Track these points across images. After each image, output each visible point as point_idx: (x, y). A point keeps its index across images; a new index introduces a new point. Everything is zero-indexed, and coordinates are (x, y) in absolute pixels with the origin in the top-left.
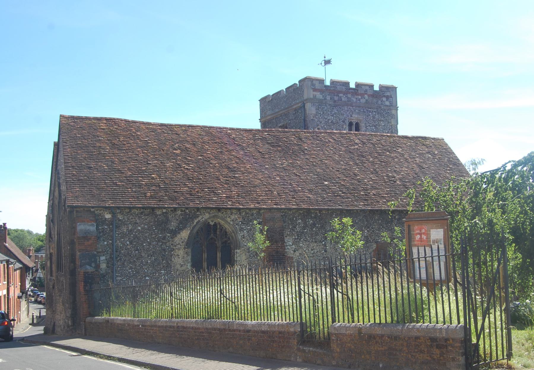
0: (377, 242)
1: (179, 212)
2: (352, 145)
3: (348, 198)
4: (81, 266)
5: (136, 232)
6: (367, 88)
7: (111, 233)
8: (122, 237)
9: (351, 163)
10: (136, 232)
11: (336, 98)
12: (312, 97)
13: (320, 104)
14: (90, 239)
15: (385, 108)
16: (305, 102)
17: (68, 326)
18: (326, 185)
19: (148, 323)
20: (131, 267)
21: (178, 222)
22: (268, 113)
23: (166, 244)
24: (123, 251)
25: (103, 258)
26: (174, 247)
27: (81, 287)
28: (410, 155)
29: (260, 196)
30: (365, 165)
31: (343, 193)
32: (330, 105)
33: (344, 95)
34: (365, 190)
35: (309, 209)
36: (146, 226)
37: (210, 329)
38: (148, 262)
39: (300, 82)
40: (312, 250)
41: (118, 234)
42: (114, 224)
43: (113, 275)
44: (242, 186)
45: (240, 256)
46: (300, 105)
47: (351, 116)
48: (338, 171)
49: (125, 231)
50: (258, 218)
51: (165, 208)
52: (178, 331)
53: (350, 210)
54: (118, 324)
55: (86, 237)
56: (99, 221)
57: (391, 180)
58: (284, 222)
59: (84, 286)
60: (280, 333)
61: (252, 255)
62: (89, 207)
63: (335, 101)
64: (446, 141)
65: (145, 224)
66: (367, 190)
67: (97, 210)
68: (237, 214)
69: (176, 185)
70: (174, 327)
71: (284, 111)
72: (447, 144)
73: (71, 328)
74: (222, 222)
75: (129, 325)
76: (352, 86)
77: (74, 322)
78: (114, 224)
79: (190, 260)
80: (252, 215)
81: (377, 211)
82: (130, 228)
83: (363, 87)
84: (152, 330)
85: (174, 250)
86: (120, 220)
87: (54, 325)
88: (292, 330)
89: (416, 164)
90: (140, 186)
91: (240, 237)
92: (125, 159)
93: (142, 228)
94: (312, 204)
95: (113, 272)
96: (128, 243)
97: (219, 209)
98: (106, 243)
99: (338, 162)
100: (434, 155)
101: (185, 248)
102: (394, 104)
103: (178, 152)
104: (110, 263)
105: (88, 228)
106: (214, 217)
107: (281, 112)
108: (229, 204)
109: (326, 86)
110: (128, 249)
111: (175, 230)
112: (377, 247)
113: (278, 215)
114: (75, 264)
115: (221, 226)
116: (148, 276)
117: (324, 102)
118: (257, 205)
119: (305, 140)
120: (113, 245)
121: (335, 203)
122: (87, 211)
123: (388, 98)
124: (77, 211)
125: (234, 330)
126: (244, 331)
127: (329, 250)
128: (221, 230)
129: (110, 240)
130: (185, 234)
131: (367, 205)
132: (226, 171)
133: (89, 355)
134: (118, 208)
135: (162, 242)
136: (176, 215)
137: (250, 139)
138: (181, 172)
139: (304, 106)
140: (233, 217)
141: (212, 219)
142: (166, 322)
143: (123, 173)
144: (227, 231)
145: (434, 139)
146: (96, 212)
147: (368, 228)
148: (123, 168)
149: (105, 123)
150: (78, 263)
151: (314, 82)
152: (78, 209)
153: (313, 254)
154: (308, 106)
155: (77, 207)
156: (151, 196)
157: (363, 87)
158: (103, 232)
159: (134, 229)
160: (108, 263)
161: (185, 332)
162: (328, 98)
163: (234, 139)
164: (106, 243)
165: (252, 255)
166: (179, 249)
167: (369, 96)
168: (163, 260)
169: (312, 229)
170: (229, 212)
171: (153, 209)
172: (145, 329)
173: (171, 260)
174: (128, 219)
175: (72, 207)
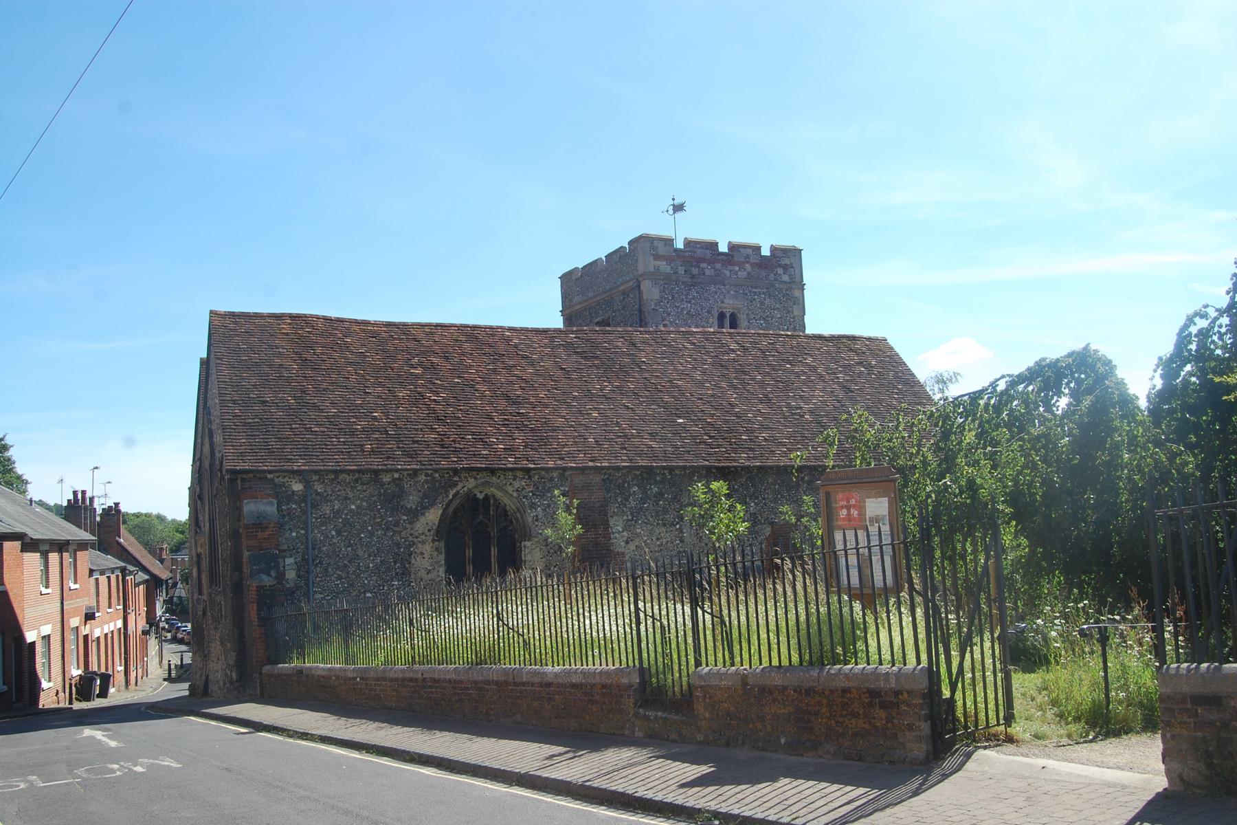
0: (772, 524)
1: (422, 478)
3: (719, 446)
6: (750, 251)
9: (724, 385)
11: (695, 271)
17: (231, 682)
18: (680, 424)
19: (372, 674)
22: (575, 300)
25: (289, 561)
27: (252, 612)
28: (827, 368)
31: (711, 437)
34: (749, 431)
35: (651, 468)
39: (630, 243)
42: (309, 501)
44: (532, 429)
45: (531, 553)
51: (397, 471)
56: (282, 495)
58: (608, 491)
62: (265, 471)
63: (693, 277)
64: (891, 342)
65: (362, 500)
70: (416, 680)
72: (892, 348)
74: (498, 494)
75: (338, 678)
76: (723, 248)
77: (241, 675)
78: (309, 501)
80: (551, 479)
81: (771, 468)
86: (318, 494)
87: (207, 681)
88: (625, 681)
90: (353, 433)
91: (530, 520)
92: (325, 385)
93: (358, 507)
95: (308, 585)
97: (492, 471)
99: (701, 384)
100: (869, 367)
101: (433, 541)
103: (418, 371)
104: (304, 568)
105: (262, 508)
106: (483, 484)
109: (677, 250)
112: (772, 531)
114: (242, 572)
115: (496, 500)
116: (369, 591)
124: (243, 480)
125: (523, 684)
126: (541, 685)
130: (433, 516)
131: (754, 458)
132: (503, 404)
134: (315, 472)
137: (545, 346)
140: (517, 484)
142: (403, 671)
145: (869, 339)
150: (246, 571)
154: (646, 285)
160: (299, 570)
162: (681, 271)
163: (516, 346)
166: (423, 543)
167: (753, 265)
168: (395, 563)
175: (234, 472)
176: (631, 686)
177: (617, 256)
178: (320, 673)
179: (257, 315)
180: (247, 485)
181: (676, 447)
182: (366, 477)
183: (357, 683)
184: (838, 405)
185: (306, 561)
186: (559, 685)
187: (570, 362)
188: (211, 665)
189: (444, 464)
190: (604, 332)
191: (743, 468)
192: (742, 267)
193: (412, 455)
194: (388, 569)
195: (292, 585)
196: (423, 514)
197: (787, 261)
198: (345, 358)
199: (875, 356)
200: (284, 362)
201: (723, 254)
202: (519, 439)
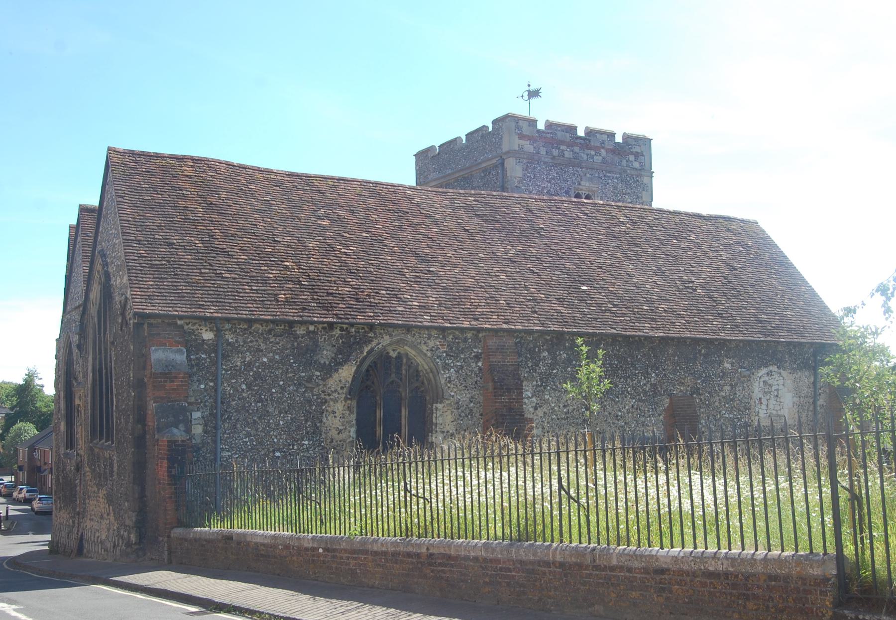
0: (670, 395)
1: (337, 332)
2: (616, 225)
3: (624, 315)
4: (159, 430)
6: (605, 137)
7: (213, 369)
8: (233, 376)
9: (619, 255)
10: (258, 368)
11: (555, 152)
12: (517, 148)
13: (531, 160)
14: (176, 378)
15: (633, 172)
16: (504, 157)
17: (129, 544)
18: (584, 291)
19: (344, 545)
21: (334, 350)
22: (431, 177)
23: (312, 391)
25: (197, 415)
26: (327, 397)
27: (160, 470)
28: (710, 246)
29: (477, 307)
30: (642, 259)
31: (615, 306)
32: (545, 163)
33: (568, 147)
34: (649, 302)
35: (562, 334)
36: (277, 357)
37: (532, 563)
38: (279, 425)
39: (495, 122)
40: (565, 406)
41: (226, 371)
42: (219, 351)
43: (216, 448)
44: (444, 288)
45: (443, 416)
46: (494, 161)
47: (580, 184)
48: (601, 268)
49: (239, 364)
50: (475, 347)
51: (312, 323)
52: (430, 564)
53: (630, 336)
54: (256, 544)
56: (192, 345)
57: (688, 287)
58: (520, 355)
59: (169, 467)
60: (771, 578)
61: (463, 414)
62: (174, 316)
63: (554, 158)
64: (763, 225)
65: (275, 353)
66: (652, 302)
68: (438, 337)
69: (330, 282)
70: (418, 555)
71: (462, 173)
72: (763, 231)
73: (135, 547)
74: (412, 353)
75: (287, 547)
76: (581, 133)
77: (141, 537)
78: (219, 351)
79: (354, 422)
81: (672, 339)
82: (247, 359)
83: (598, 136)
84: (355, 559)
85: (326, 402)
86: (229, 344)
87: (81, 539)
88: (816, 572)
89: (722, 261)
90: (265, 281)
91: (443, 381)
92: (232, 231)
93: (270, 360)
94: (565, 323)
95: (215, 442)
96: (244, 387)
97: (408, 329)
98: (202, 386)
99: (598, 253)
100: (746, 246)
101: (346, 399)
102: (647, 167)
103: (326, 223)
104: (211, 424)
106: (398, 342)
107: (457, 175)
108: (426, 320)
109: (539, 131)
111: (330, 364)
112: (671, 403)
113: (511, 342)
114: (144, 425)
115: (408, 359)
116: (279, 450)
117: (536, 158)
118: (473, 323)
119: (538, 213)
120: (216, 390)
121: (604, 323)
122: (169, 324)
123: (637, 155)
124: (150, 325)
125: (612, 569)
126: (646, 571)
128: (410, 366)
129: (211, 381)
130: (347, 373)
131: (657, 329)
132: (413, 260)
133: (229, 612)
134: (228, 320)
135: (306, 387)
136: (332, 336)
137: (446, 207)
138: (335, 260)
139: (503, 164)
140: (431, 343)
141: (393, 347)
142: (395, 544)
143: (231, 257)
144: (420, 368)
145: (742, 221)
146: (186, 327)
147: (657, 369)
148: (232, 247)
149: (192, 167)
150: (151, 423)
152: (152, 321)
153: (566, 413)
154: (510, 163)
155: (150, 316)
157: (598, 136)
158: (197, 365)
159: (255, 362)
160: (206, 425)
161: (452, 566)
162: (543, 151)
163: (418, 205)
164: (202, 386)
165: (463, 414)
166: (335, 401)
167: (607, 151)
168: (306, 421)
169: (565, 368)
170: (425, 334)
171: (291, 324)
172: (334, 557)
173: (321, 422)
174: (245, 342)
175: (142, 317)
176: (826, 580)
177: (478, 136)
178: (258, 540)
179: (157, 156)
181: (583, 313)
182: (280, 328)
183: (319, 555)
184: (725, 281)
186: (681, 572)
187: (474, 223)
188: (89, 524)
189: (360, 319)
190: (502, 198)
191: (646, 338)
192: (598, 153)
193: (328, 307)
194: (299, 428)
195: (199, 441)
196: (336, 371)
197: (637, 149)
198: (251, 205)
199: (751, 237)
200: (189, 204)
201: (580, 138)
202: (433, 297)
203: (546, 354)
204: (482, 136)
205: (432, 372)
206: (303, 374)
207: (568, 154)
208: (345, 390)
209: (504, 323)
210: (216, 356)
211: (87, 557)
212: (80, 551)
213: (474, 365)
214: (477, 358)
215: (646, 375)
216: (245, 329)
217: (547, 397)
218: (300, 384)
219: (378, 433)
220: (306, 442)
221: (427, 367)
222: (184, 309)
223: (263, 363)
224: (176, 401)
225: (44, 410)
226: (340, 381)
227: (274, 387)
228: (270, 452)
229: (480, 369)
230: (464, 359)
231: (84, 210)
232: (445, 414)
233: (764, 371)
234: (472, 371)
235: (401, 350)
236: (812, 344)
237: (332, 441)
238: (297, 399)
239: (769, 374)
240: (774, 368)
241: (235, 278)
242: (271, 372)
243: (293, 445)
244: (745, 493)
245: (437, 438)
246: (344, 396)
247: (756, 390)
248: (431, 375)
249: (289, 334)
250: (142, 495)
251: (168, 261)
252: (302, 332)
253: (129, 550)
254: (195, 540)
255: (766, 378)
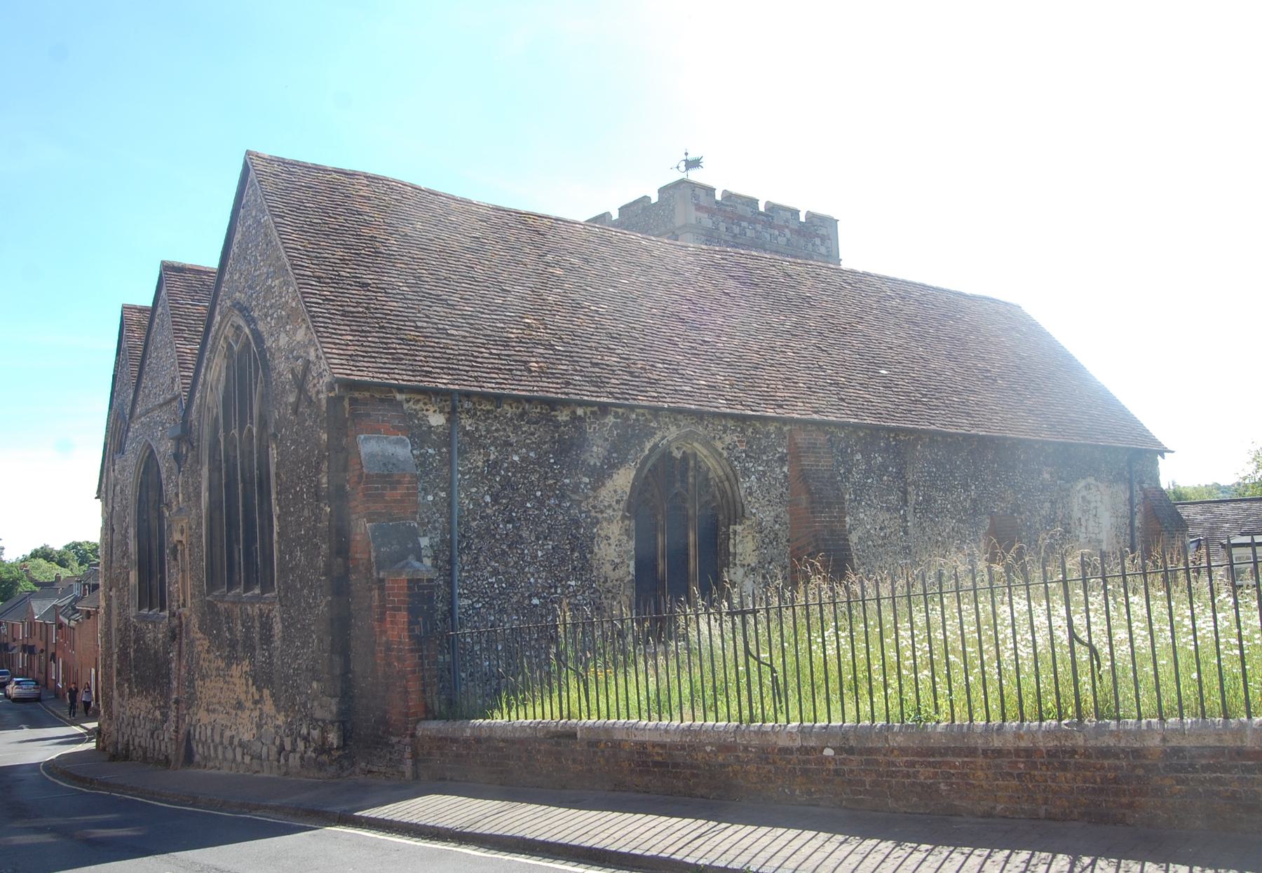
1: (610, 420)
5: (507, 470)
6: (788, 215)
8: (474, 483)
10: (507, 470)
11: (736, 230)
12: (694, 222)
14: (399, 482)
20: (495, 569)
24: (474, 524)
26: (600, 516)
31: (925, 396)
38: (536, 556)
39: (661, 191)
40: (881, 529)
41: (463, 474)
49: (480, 464)
55: (389, 476)
59: (410, 623)
61: (767, 540)
63: (735, 236)
67: (408, 401)
69: (590, 348)
73: (336, 754)
80: (768, 435)
82: (492, 457)
86: (467, 433)
87: (189, 737)
92: (444, 273)
93: (523, 460)
96: (488, 499)
98: (430, 498)
101: (624, 518)
105: (391, 449)
109: (717, 202)
110: (488, 516)
111: (602, 467)
113: (822, 439)
116: (537, 595)
127: (911, 531)
129: (443, 490)
130: (623, 480)
134: (468, 395)
135: (571, 500)
140: (728, 439)
146: (406, 406)
151: (697, 191)
152: (356, 395)
153: (884, 538)
156: (542, 371)
162: (722, 227)
164: (430, 498)
165: (767, 540)
166: (610, 520)
168: (573, 550)
171: (552, 404)
173: (591, 552)
174: (488, 431)
180: (362, 410)
185: (450, 544)
192: (782, 234)
193: (599, 383)
196: (610, 476)
197: (823, 231)
201: (761, 214)
203: (859, 457)
204: (644, 209)
205: (728, 479)
206: (567, 481)
207: (750, 233)
208: (622, 505)
209: (816, 412)
210: (450, 452)
211: (199, 766)
212: (189, 758)
213: (778, 470)
214: (782, 460)
215: (966, 487)
216: (488, 412)
217: (862, 516)
218: (563, 496)
219: (660, 568)
220: (573, 583)
221: (721, 473)
222: (406, 377)
223: (513, 463)
224: (400, 519)
225: (6, 576)
226: (615, 491)
227: (529, 500)
228: (524, 598)
229: (786, 476)
230: (767, 461)
231: (170, 272)
232: (746, 540)
233: (1082, 483)
234: (775, 479)
235: (687, 448)
236: (1128, 449)
237: (606, 581)
238: (561, 518)
239: (1088, 487)
240: (1091, 480)
241: (465, 337)
242: (525, 478)
243: (556, 587)
244: (875, 650)
245: (734, 574)
246: (621, 513)
247: (1076, 508)
248: (726, 484)
249: (548, 421)
250: (346, 670)
251: (367, 308)
252: (565, 418)
253: (324, 758)
254: (478, 740)
255: (1084, 493)
